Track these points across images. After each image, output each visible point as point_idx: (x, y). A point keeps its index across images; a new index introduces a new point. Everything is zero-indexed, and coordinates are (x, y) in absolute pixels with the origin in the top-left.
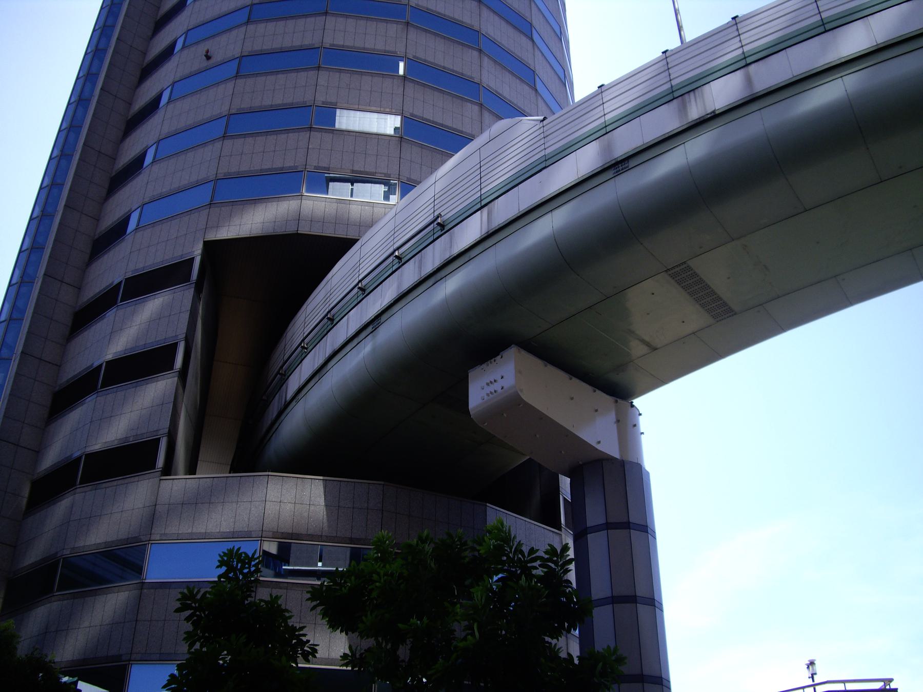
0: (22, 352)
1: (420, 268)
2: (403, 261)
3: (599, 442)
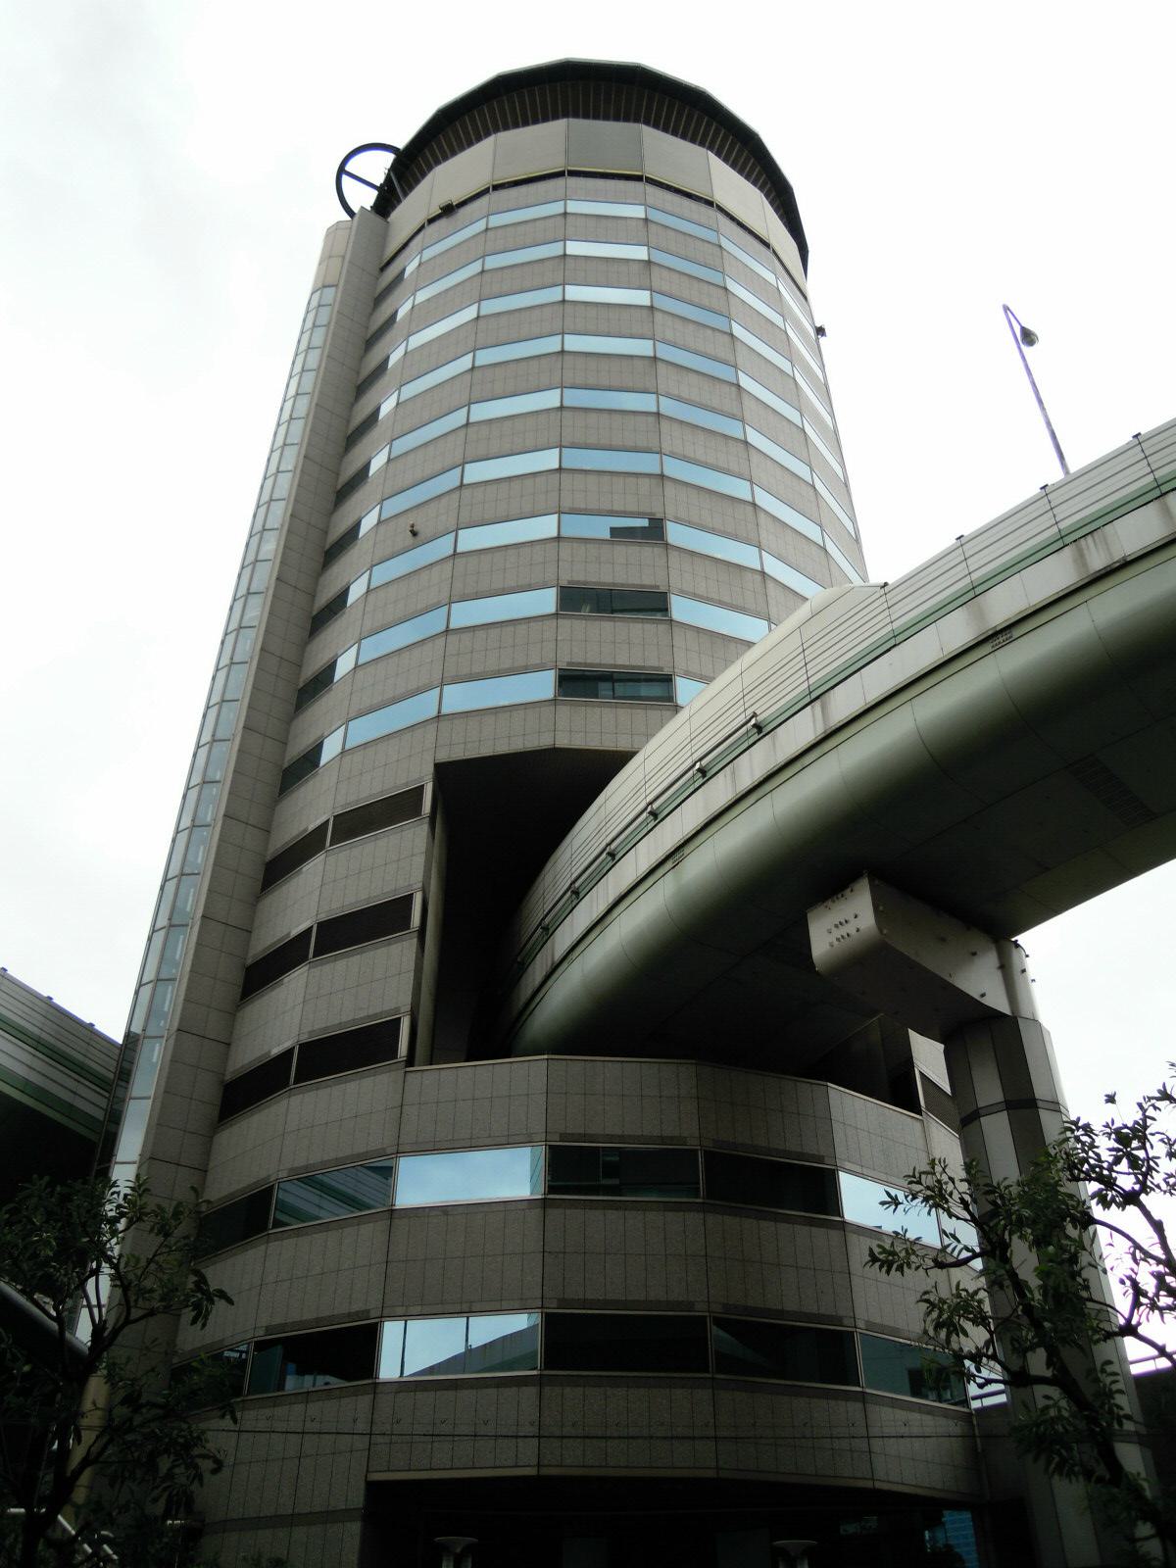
0: (203, 916)
1: (734, 780)
2: (709, 775)
3: (983, 995)
